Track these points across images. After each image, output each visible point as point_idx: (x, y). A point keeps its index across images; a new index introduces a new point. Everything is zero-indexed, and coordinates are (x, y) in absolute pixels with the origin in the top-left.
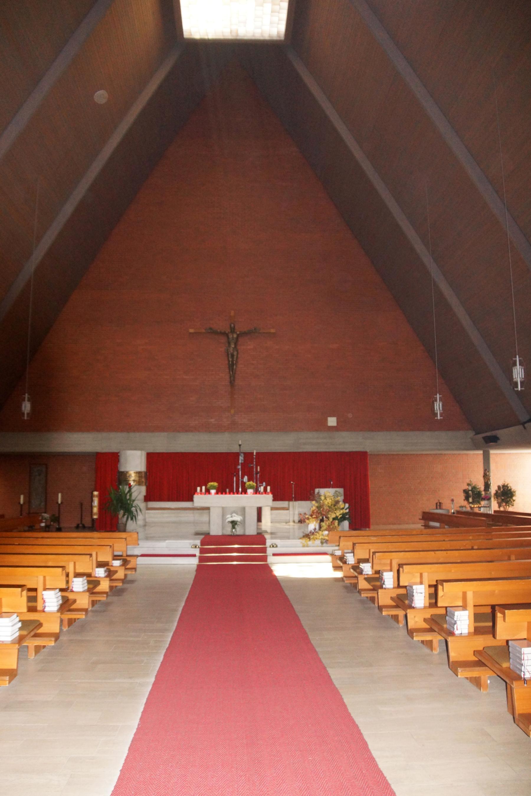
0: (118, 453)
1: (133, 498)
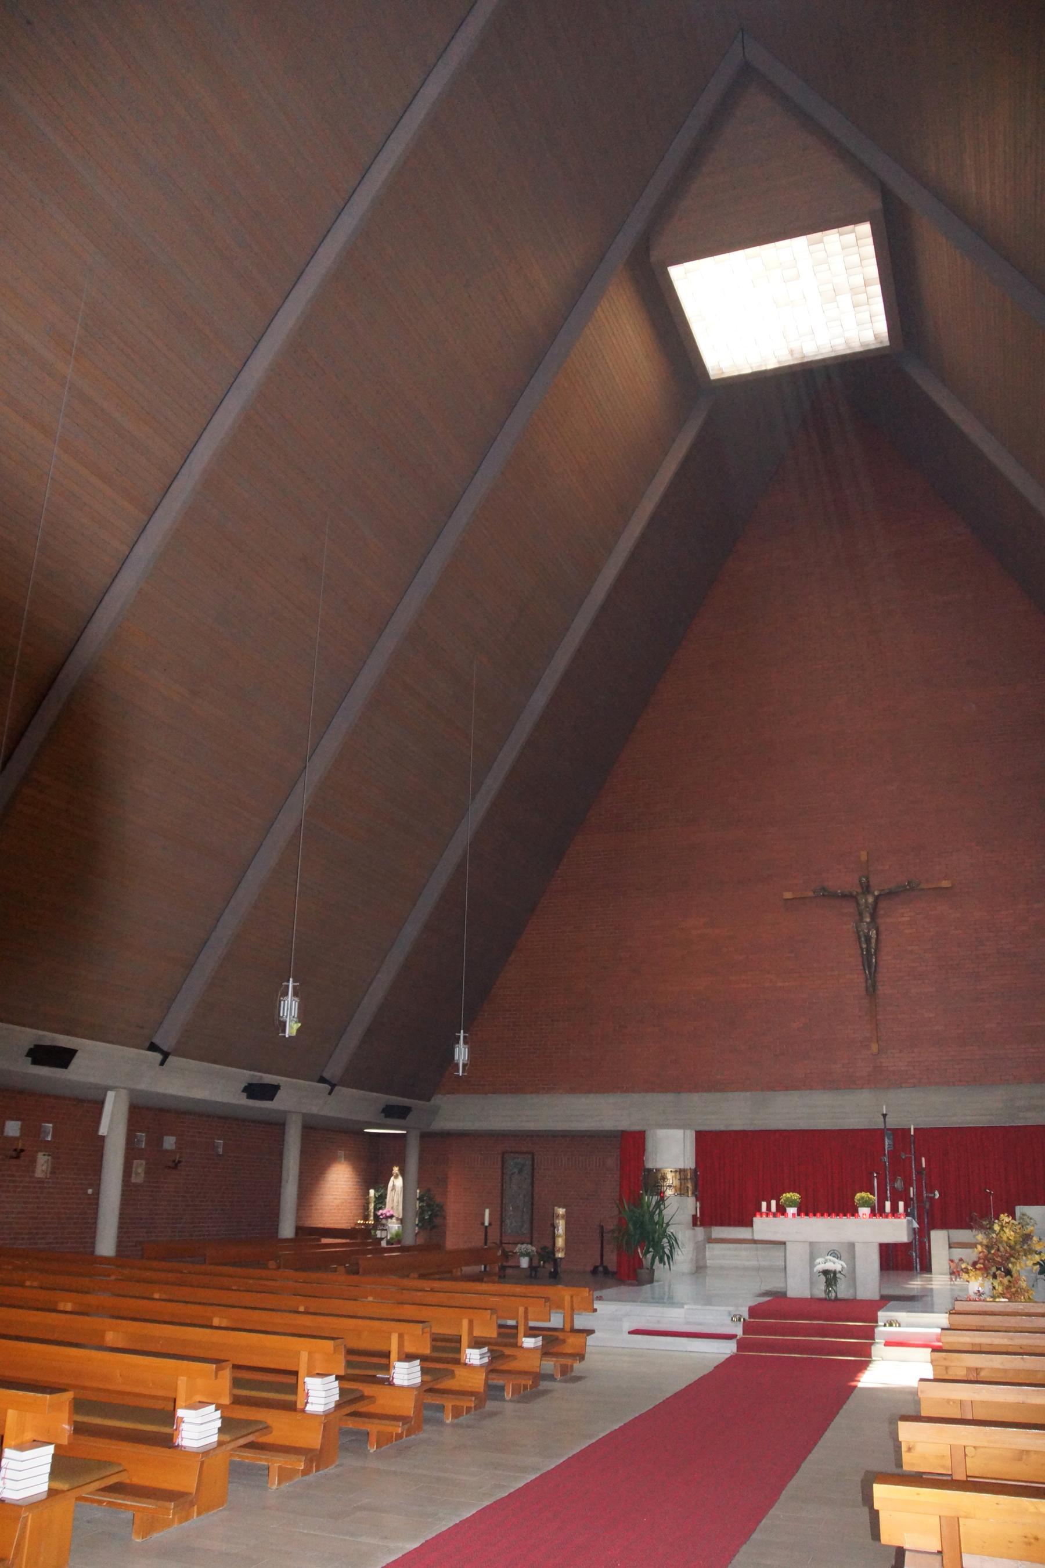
0: (645, 1131)
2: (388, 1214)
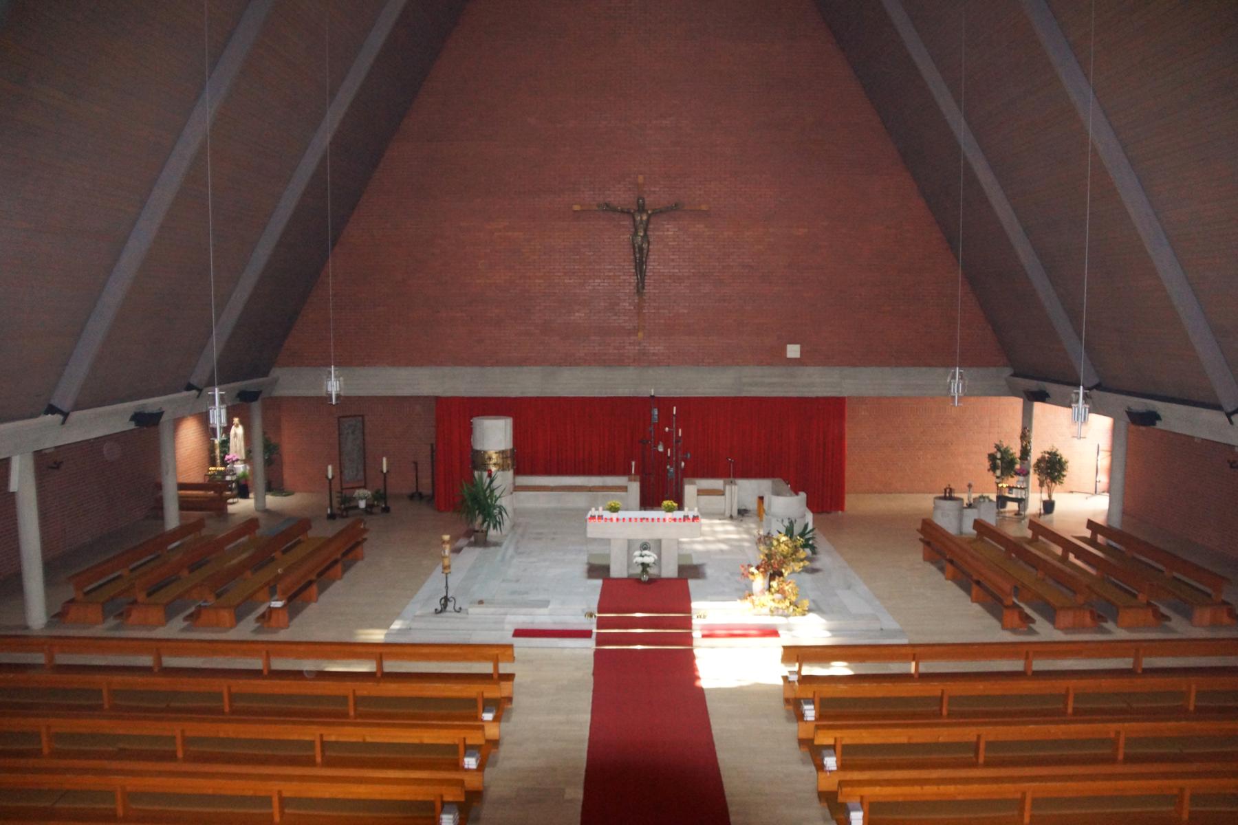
1: (497, 493)
2: (234, 459)
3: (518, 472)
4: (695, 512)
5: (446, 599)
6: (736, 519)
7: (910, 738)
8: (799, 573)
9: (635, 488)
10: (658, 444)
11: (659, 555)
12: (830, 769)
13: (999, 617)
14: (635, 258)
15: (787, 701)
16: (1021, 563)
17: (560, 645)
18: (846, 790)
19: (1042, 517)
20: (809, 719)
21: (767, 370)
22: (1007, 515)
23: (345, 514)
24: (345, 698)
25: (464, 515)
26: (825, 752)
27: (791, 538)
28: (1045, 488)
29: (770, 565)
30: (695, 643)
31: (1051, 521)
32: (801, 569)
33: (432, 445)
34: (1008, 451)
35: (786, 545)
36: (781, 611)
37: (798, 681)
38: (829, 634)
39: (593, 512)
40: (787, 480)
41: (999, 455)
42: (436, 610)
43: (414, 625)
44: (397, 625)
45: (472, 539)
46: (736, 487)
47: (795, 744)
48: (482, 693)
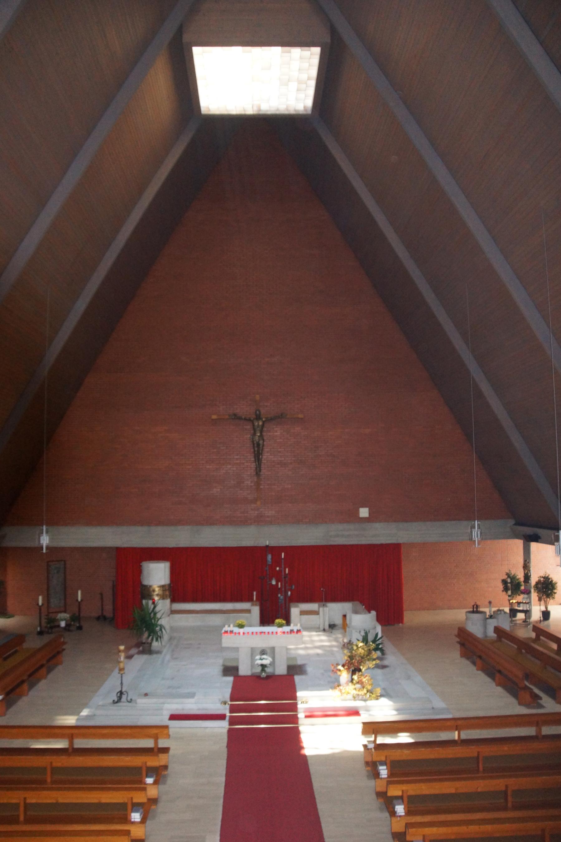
1: (158, 616)
3: (173, 601)
4: (299, 627)
5: (121, 693)
6: (328, 631)
7: (457, 789)
8: (373, 668)
9: (256, 610)
10: (272, 579)
11: (274, 658)
12: (400, 814)
13: (515, 695)
14: (255, 451)
15: (367, 763)
16: (529, 656)
17: (203, 726)
18: (412, 831)
19: (542, 623)
20: (383, 776)
21: (346, 526)
22: (518, 622)
23: (50, 631)
24: (45, 769)
25: (135, 631)
26: (395, 802)
27: (366, 644)
28: (542, 602)
29: (352, 663)
30: (300, 722)
31: (548, 626)
32: (374, 666)
33: (113, 581)
34: (516, 577)
35: (363, 649)
36: (361, 697)
37: (374, 748)
38: (395, 712)
39: (226, 628)
40: (362, 602)
41: (509, 580)
42: (114, 701)
43: (98, 712)
44: (85, 712)
45: (141, 648)
46: (327, 609)
47: (374, 796)
48: (146, 762)
